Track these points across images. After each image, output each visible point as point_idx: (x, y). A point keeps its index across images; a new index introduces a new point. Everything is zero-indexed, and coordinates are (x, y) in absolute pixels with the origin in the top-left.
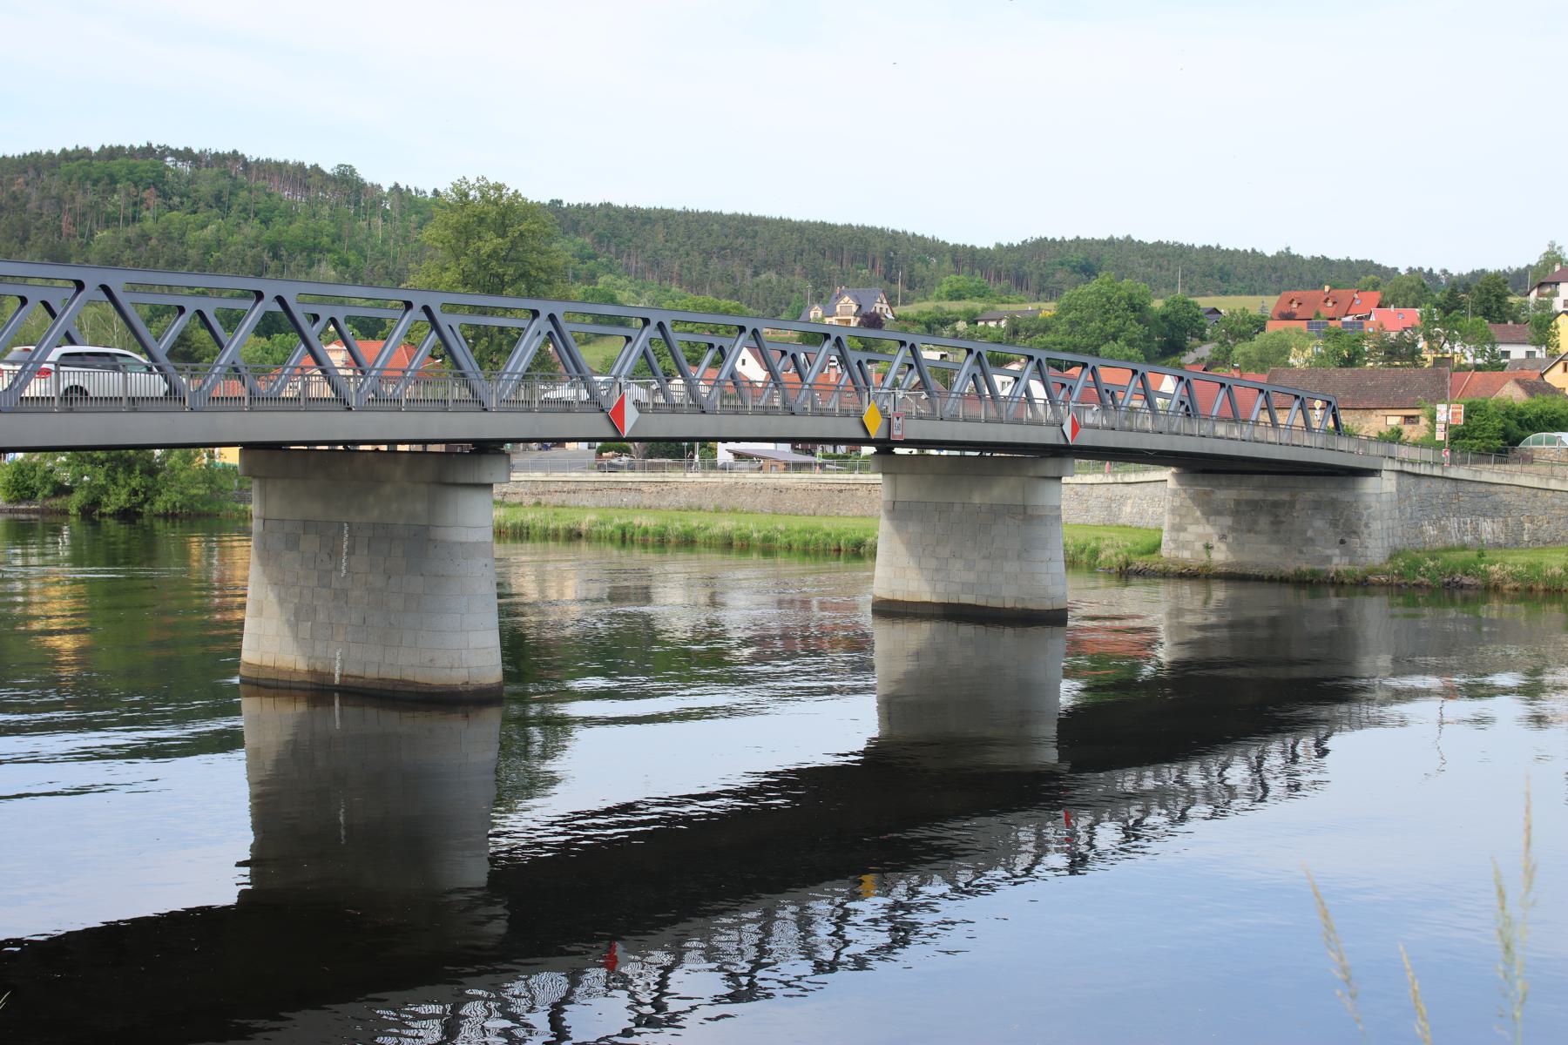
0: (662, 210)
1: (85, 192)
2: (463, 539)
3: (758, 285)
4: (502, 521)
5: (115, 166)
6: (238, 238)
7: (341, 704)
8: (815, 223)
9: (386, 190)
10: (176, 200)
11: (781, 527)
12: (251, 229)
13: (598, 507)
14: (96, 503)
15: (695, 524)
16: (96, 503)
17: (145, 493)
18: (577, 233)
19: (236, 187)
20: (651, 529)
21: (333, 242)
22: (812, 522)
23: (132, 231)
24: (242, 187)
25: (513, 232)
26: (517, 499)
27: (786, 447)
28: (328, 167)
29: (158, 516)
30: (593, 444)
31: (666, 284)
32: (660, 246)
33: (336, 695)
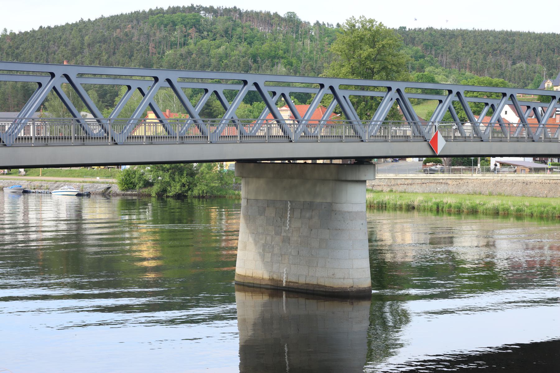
0: (461, 30)
1: (161, 31)
2: (350, 210)
3: (515, 70)
4: (372, 200)
5: (175, 17)
6: (236, 52)
7: (286, 297)
8: (549, 34)
9: (312, 24)
10: (205, 33)
11: (527, 203)
12: (243, 47)
13: (424, 193)
14: (165, 191)
15: (477, 202)
16: (165, 191)
17: (188, 186)
18: (414, 44)
19: (236, 25)
20: (453, 205)
21: (285, 53)
22: (545, 201)
23: (184, 50)
24: (238, 25)
25: (379, 45)
26: (379, 189)
27: (530, 159)
28: (282, 14)
29: (195, 197)
30: (421, 159)
31: (463, 71)
32: (460, 50)
33: (284, 293)
